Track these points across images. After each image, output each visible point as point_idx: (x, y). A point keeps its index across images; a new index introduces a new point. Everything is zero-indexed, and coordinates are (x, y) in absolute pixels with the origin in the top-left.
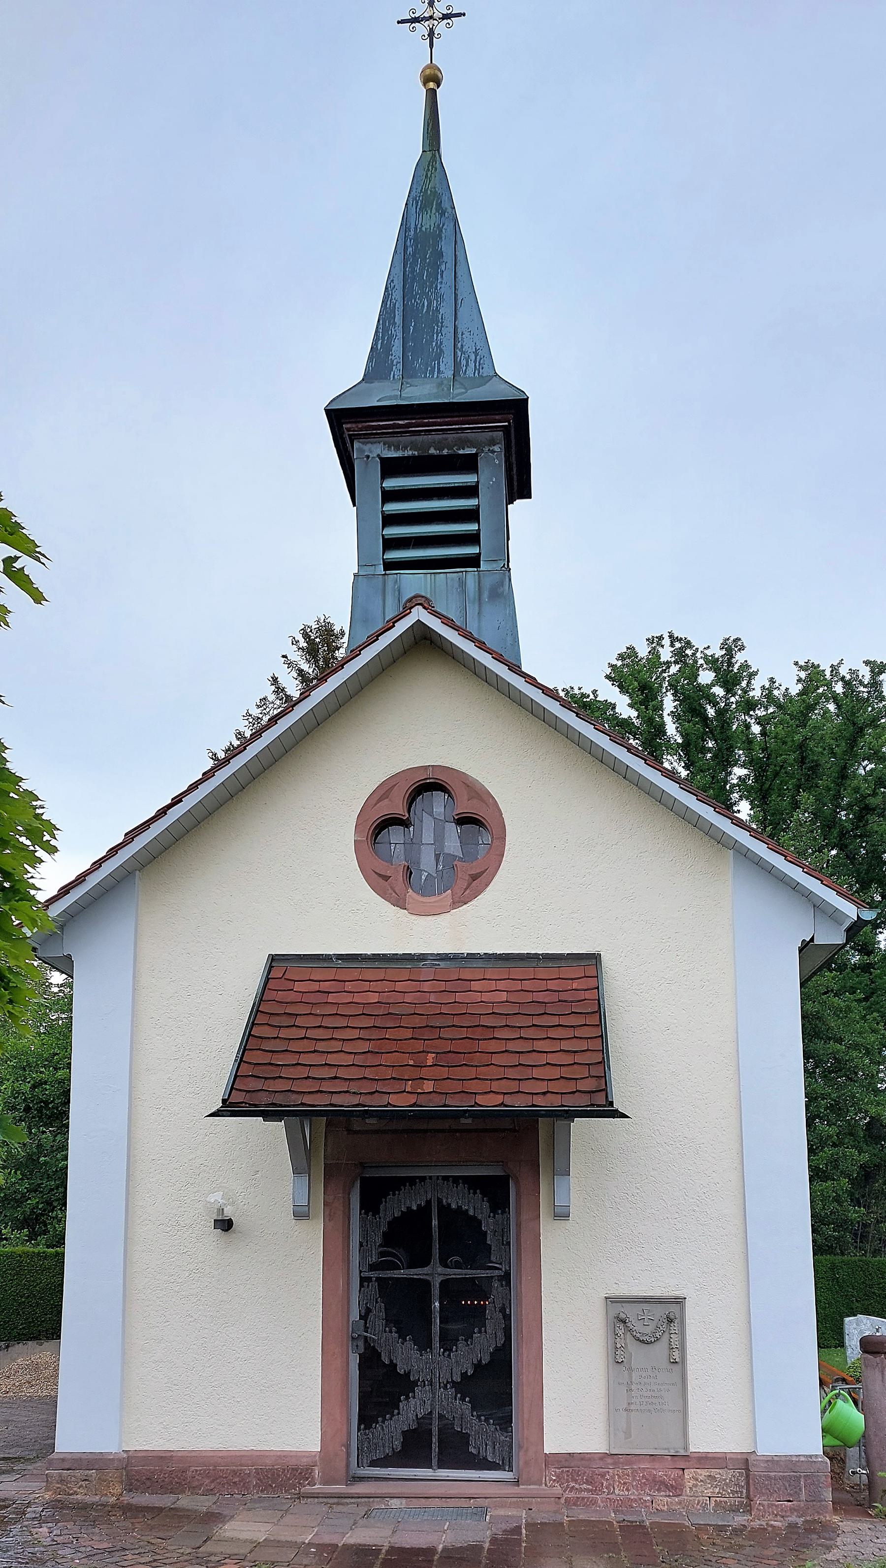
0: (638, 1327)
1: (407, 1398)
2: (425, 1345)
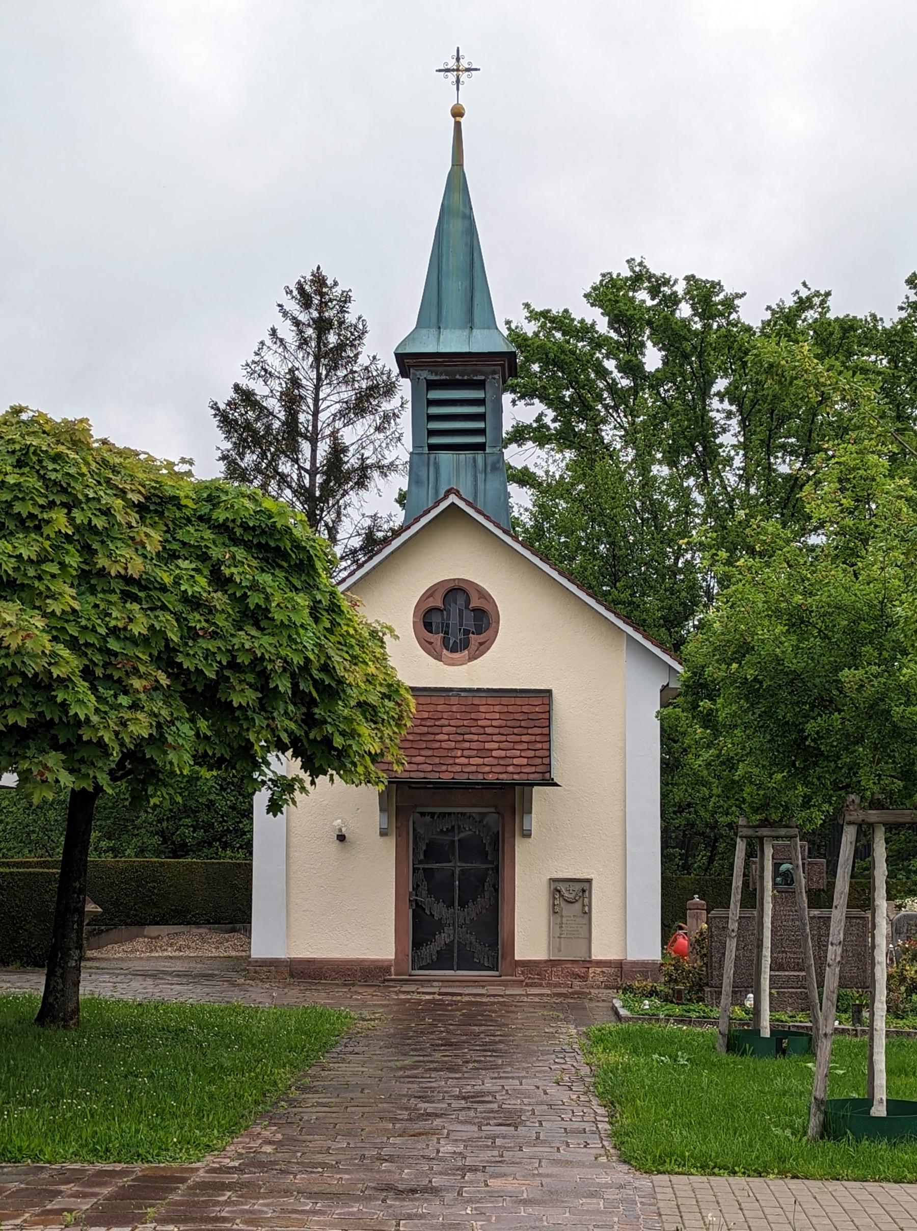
1: (440, 933)
2: (451, 905)
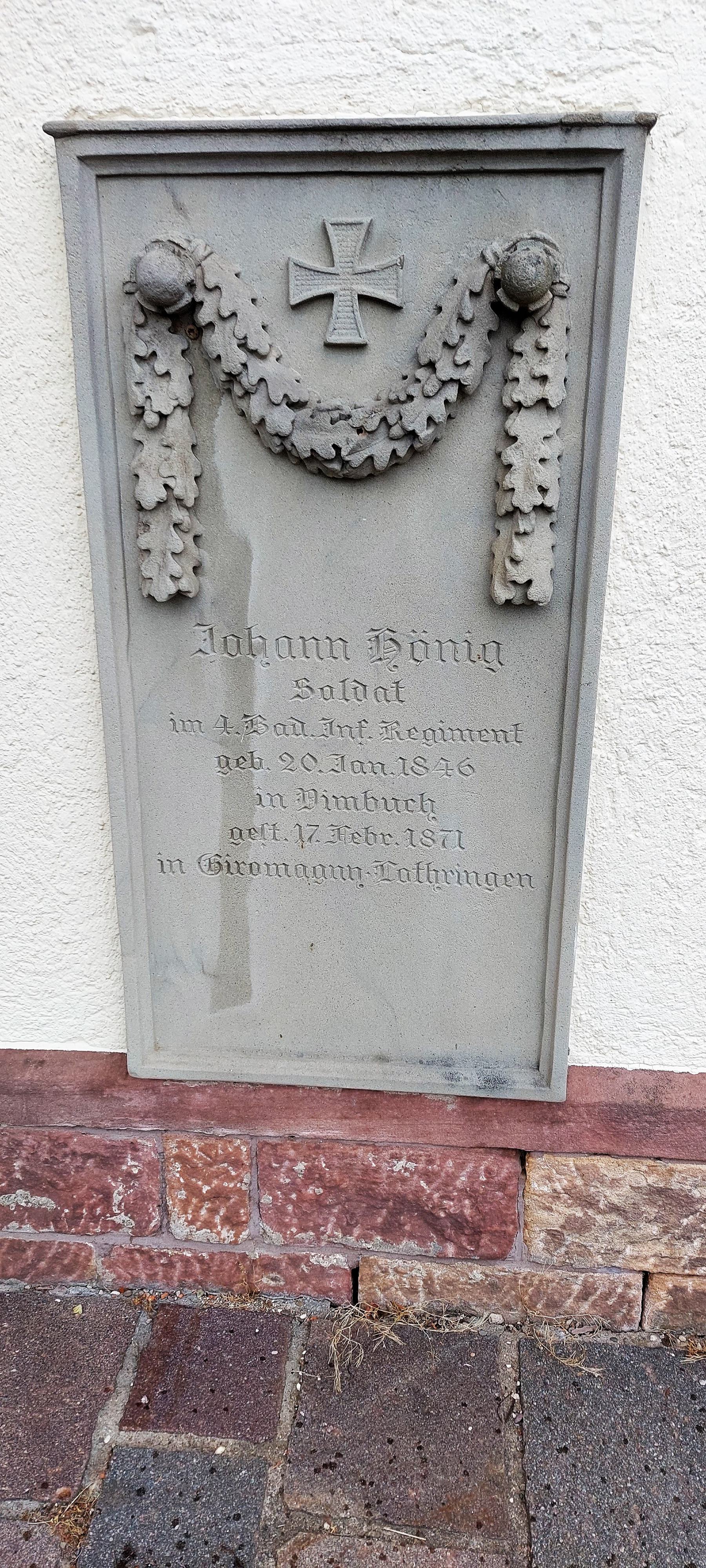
0: (292, 362)
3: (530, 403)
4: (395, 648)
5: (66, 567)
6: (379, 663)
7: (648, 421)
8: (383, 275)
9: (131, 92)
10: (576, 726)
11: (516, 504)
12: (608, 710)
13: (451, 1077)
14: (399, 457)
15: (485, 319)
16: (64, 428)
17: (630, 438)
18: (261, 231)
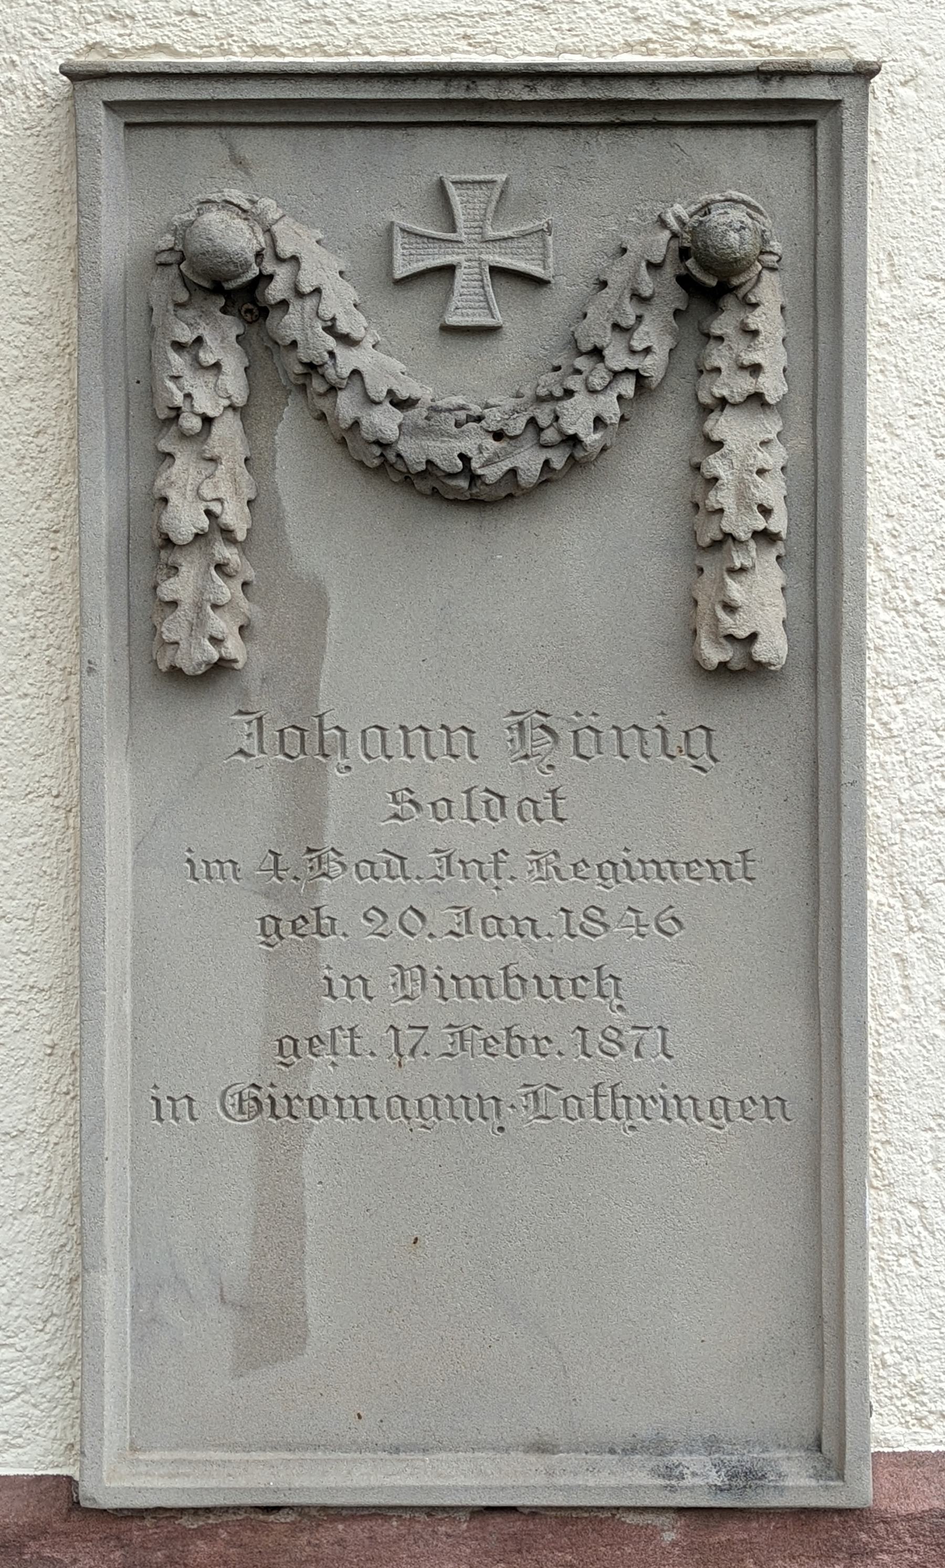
3: (739, 399)
4: (549, 738)
5: (26, 635)
6: (524, 762)
7: (902, 424)
8: (524, 242)
9: (172, 28)
10: (839, 847)
11: (727, 529)
12: (884, 830)
13: (669, 1472)
14: (555, 470)
15: (674, 297)
16: (41, 440)
17: (878, 445)
18: (352, 190)
